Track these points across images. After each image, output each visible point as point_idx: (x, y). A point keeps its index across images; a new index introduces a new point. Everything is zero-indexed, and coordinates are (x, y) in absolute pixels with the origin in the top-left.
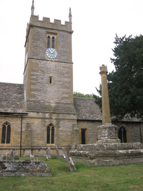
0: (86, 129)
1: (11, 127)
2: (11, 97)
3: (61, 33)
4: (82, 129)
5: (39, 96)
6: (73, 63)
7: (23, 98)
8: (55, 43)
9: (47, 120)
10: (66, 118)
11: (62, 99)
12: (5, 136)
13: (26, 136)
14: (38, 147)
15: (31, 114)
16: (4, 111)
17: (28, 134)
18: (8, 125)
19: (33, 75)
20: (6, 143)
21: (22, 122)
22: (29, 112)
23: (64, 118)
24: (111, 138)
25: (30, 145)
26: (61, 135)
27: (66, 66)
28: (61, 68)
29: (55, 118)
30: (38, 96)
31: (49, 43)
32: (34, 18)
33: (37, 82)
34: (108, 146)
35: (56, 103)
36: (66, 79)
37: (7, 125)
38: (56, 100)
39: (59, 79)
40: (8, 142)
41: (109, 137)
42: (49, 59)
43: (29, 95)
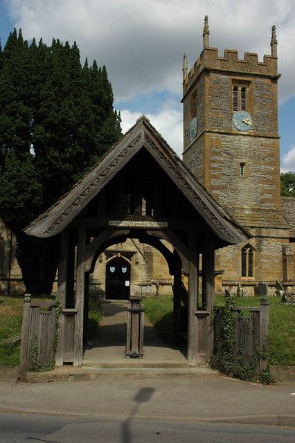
8: (247, 99)
19: (214, 161)
31: (236, 103)
42: (239, 132)
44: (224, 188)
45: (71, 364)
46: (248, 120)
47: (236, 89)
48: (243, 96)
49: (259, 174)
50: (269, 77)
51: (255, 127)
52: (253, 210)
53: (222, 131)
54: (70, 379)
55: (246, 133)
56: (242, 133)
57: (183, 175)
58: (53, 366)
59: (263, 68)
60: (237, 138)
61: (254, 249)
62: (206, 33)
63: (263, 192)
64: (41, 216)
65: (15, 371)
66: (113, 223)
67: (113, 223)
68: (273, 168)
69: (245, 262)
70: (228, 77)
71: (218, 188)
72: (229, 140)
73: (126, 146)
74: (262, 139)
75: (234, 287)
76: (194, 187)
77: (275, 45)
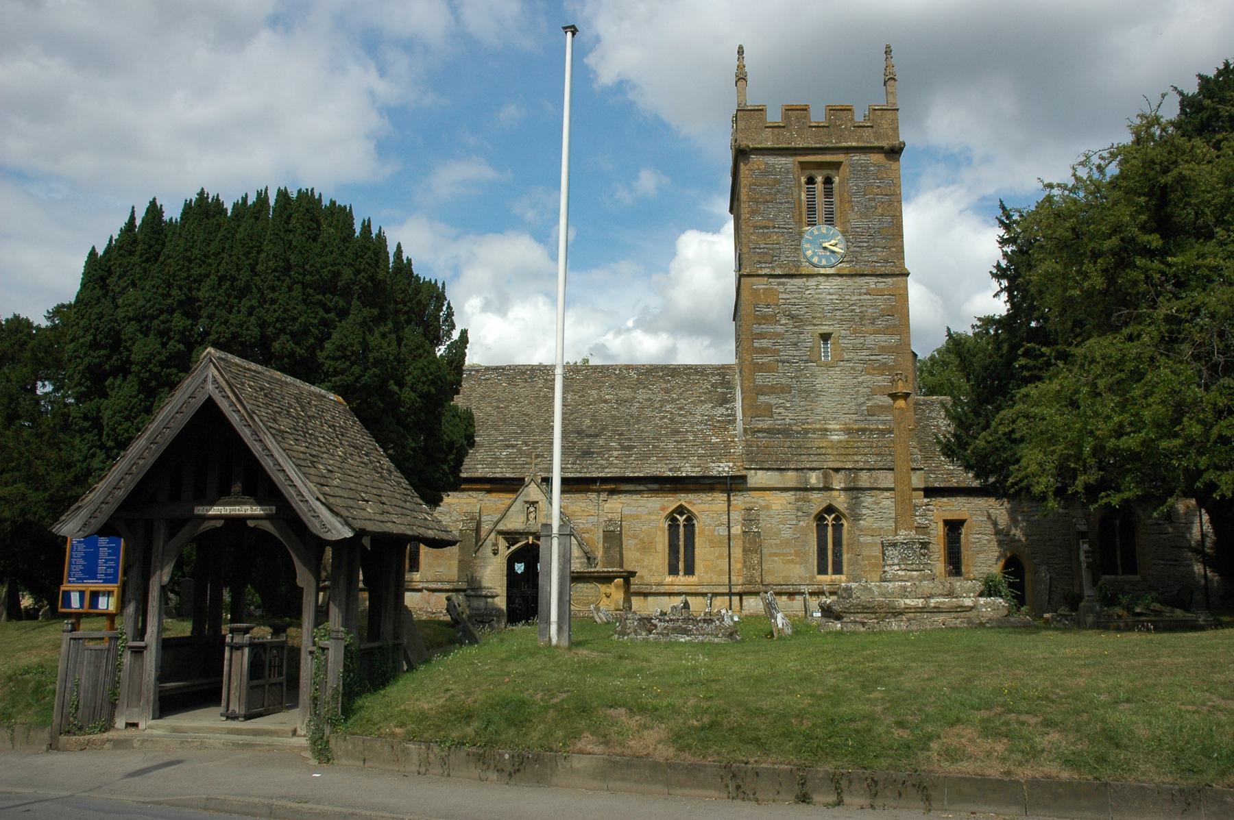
0: (961, 522)
2: (690, 418)
5: (786, 408)
6: (908, 275)
8: (836, 199)
9: (815, 496)
15: (758, 478)
16: (670, 470)
19: (761, 336)
20: (681, 573)
21: (729, 506)
23: (875, 485)
27: (881, 286)
29: (843, 485)
31: (811, 209)
32: (746, 114)
36: (883, 339)
40: (690, 570)
43: (753, 411)
44: (785, 390)
45: (135, 725)
46: (836, 243)
47: (811, 181)
48: (829, 193)
50: (880, 150)
51: (851, 255)
52: (848, 431)
53: (778, 272)
54: (106, 746)
55: (832, 271)
56: (822, 271)
57: (261, 435)
58: (109, 726)
59: (867, 133)
60: (812, 282)
61: (844, 515)
62: (741, 78)
63: (873, 392)
64: (73, 508)
65: (45, 735)
66: (200, 510)
67: (200, 510)
68: (894, 340)
69: (826, 556)
70: (791, 159)
71: (772, 390)
72: (794, 288)
73: (187, 396)
74: (867, 279)
75: (797, 597)
76: (276, 455)
77: (892, 82)
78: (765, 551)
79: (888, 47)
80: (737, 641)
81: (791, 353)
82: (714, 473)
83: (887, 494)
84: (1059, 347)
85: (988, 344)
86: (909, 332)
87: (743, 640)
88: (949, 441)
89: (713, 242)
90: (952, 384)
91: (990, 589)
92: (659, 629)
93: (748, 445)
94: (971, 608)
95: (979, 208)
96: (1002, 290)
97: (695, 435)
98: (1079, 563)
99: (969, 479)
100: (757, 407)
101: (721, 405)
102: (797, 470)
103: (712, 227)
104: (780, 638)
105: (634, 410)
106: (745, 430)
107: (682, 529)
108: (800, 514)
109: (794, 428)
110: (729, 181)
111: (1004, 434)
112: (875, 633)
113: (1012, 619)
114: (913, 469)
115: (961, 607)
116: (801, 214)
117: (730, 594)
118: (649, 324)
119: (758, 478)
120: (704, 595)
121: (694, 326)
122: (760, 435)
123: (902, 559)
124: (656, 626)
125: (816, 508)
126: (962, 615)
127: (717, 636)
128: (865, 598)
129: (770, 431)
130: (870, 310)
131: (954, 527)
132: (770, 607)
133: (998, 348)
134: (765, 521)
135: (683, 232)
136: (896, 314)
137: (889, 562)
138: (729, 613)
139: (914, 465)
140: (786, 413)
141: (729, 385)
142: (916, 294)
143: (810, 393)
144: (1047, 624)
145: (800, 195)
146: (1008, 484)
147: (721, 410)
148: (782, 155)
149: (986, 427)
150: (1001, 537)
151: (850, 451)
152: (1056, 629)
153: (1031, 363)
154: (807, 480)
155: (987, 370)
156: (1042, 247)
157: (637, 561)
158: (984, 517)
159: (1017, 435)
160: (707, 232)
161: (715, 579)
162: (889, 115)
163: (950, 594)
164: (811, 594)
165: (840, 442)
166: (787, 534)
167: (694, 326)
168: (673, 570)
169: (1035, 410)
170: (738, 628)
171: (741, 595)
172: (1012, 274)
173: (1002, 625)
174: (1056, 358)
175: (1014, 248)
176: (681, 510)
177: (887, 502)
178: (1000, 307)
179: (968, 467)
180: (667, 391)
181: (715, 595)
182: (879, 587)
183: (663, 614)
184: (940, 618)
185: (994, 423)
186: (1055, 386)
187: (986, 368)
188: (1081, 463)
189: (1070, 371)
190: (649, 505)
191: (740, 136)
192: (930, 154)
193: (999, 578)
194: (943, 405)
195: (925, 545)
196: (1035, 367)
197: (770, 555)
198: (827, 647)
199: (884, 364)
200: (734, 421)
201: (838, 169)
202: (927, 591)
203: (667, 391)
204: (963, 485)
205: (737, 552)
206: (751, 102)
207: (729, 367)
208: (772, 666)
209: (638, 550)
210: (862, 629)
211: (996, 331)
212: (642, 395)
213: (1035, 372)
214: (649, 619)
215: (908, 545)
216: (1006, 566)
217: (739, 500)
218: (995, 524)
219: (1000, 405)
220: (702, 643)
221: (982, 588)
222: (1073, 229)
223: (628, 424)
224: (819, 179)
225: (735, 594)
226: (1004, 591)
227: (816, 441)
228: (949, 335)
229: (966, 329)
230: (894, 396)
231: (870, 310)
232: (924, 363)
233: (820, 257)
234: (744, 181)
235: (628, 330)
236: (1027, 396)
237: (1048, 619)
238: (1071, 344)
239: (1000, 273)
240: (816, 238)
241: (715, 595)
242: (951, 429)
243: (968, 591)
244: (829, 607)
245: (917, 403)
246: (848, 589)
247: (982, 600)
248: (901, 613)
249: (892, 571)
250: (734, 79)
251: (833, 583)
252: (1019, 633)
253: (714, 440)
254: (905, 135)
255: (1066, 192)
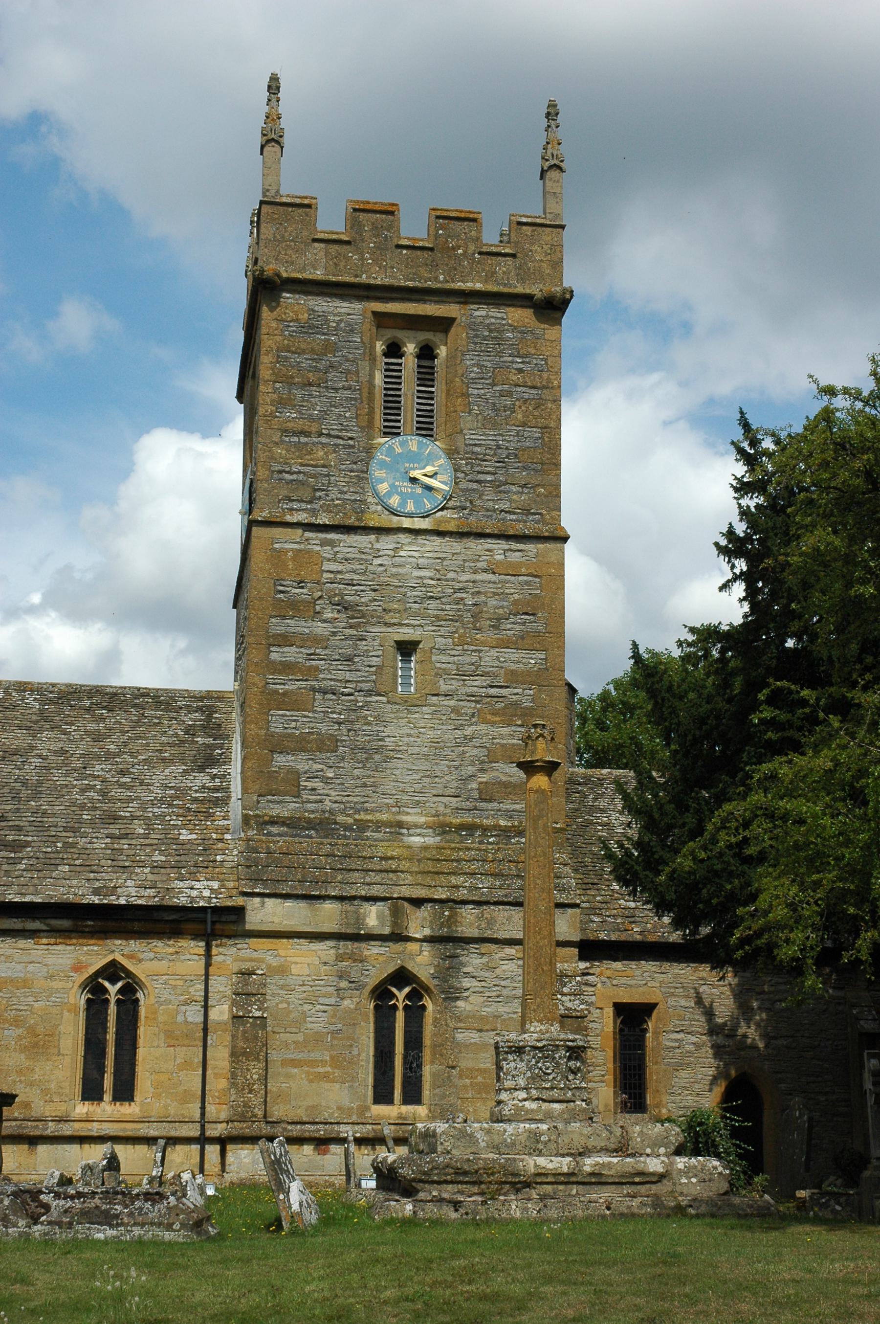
0: (648, 1009)
1: (140, 995)
2: (140, 792)
3: (480, 312)
4: (620, 1009)
5: (326, 781)
6: (565, 539)
7: (218, 798)
8: (439, 389)
9: (374, 950)
10: (500, 935)
11: (482, 800)
12: (103, 1054)
13: (235, 1055)
14: (313, 1127)
15: (264, 913)
16: (96, 892)
17: (246, 1039)
18: (120, 984)
19: (285, 640)
20: (107, 1097)
21: (208, 965)
22: (257, 900)
23: (488, 934)
24: (544, 1101)
25: (260, 1114)
26: (466, 1046)
27: (515, 557)
28: (478, 577)
29: (427, 932)
30: (317, 784)
31: (392, 404)
32: (277, 212)
33: (313, 690)
34: (496, 1137)
35: (443, 828)
36: (514, 659)
37: (113, 982)
38: (445, 807)
39: (467, 659)
40: (125, 1091)
41: (534, 1092)
42: (395, 522)
43: (264, 781)
44: (326, 745)
46: (434, 468)
47: (394, 350)
48: (426, 376)
49: (476, 685)
50: (525, 301)
51: (462, 497)
52: (443, 828)
53: (324, 519)
55: (424, 524)
56: (406, 523)
59: (503, 266)
60: (386, 543)
61: (427, 990)
62: (272, 140)
63: (492, 758)
68: (533, 660)
69: (392, 1043)
71: (299, 744)
72: (353, 553)
74: (489, 544)
75: (333, 1148)
77: (553, 174)
78: (274, 1056)
79: (552, 105)
80: (210, 1239)
81: (341, 675)
82: (183, 901)
83: (510, 951)
84: (832, 689)
85: (708, 675)
86: (562, 647)
87: (220, 1237)
88: (628, 854)
89: (201, 455)
90: (639, 746)
91: (696, 1140)
92: (54, 1214)
93: (250, 848)
94: (661, 1177)
95: (701, 419)
96: (735, 578)
97: (149, 827)
98: (863, 1094)
99: (662, 928)
100: (272, 776)
101: (201, 769)
102: (341, 899)
103: (208, 427)
104: (293, 1233)
105: (31, 770)
106: (246, 819)
107: (112, 1009)
108: (344, 984)
109: (340, 819)
110: (239, 337)
111: (730, 846)
112: (477, 1224)
113: (736, 1200)
114: (559, 905)
115: (641, 1174)
116: (371, 413)
117: (203, 1140)
118: (71, 601)
119: (264, 913)
120: (150, 1141)
121: (160, 612)
122: (275, 829)
123: (533, 1078)
124: (47, 1207)
125: (375, 975)
126: (643, 1189)
127: (169, 1227)
128: (460, 1153)
129: (292, 824)
130: (493, 602)
131: (633, 1017)
132: (278, 1169)
133: (726, 684)
134: (278, 1000)
135: (144, 429)
136: (541, 611)
137: (508, 1084)
138: (195, 1176)
139: (563, 898)
140: (327, 789)
141: (216, 731)
142: (579, 571)
143: (373, 754)
144: (802, 1213)
145: (372, 376)
146: (733, 940)
147: (201, 779)
148: (342, 297)
149: (697, 832)
150: (720, 1040)
151: (445, 867)
152: (818, 1221)
153: (783, 716)
154: (359, 920)
155: (697, 724)
156: (811, 502)
157: (20, 1072)
158: (687, 998)
159: (752, 850)
160: (191, 430)
161: (174, 1110)
162: (547, 235)
163: (622, 1149)
164: (360, 1142)
165: (425, 848)
166: (317, 1023)
167: (160, 612)
168: (91, 1091)
169: (785, 804)
170: (214, 1211)
171: (223, 1142)
172: (754, 549)
173: (716, 1211)
174: (827, 712)
175: (761, 500)
176: (113, 971)
177: (509, 965)
178: (730, 609)
179: (661, 907)
180: (97, 737)
181: (173, 1141)
182: (488, 1132)
183: (66, 1181)
184: (602, 1195)
185: (710, 827)
186: (823, 761)
187: (702, 721)
188: (867, 907)
189: (853, 736)
190: (51, 960)
191: (264, 253)
192: (615, 311)
193: (715, 1118)
194: (620, 787)
195: (576, 1052)
196: (789, 725)
197: (285, 1063)
198: (385, 1251)
199: (515, 704)
200: (225, 801)
201: (446, 331)
202: (578, 1143)
203: (97, 737)
204: (651, 938)
205: (220, 1057)
206: (290, 188)
207: (220, 696)
208: (276, 1291)
209: (23, 1049)
210: (454, 1215)
211: (723, 651)
212: (48, 741)
213: (790, 733)
214: (35, 1194)
215: (544, 1051)
216: (728, 1097)
217: (229, 955)
218: (709, 1014)
219: (723, 792)
220: (140, 1242)
221: (681, 1138)
222: (868, 474)
223: (16, 797)
224: (410, 348)
225: (213, 1140)
226: (724, 1144)
227: (381, 845)
228: (636, 656)
229: (667, 642)
230: (529, 768)
231: (493, 602)
232: (588, 704)
233: (404, 497)
234: (267, 342)
235: (32, 610)
236: (773, 777)
237: (803, 1201)
238: (854, 685)
239: (734, 546)
240: (398, 459)
241: (173, 1141)
242: (633, 833)
243: (655, 1145)
244: (392, 1169)
245: (572, 781)
246: (429, 1136)
247: (681, 1162)
248: (527, 1185)
249: (512, 1101)
250: (258, 140)
251: (401, 1122)
252: (750, 1228)
253: (185, 835)
254: (572, 277)
255: (859, 405)
